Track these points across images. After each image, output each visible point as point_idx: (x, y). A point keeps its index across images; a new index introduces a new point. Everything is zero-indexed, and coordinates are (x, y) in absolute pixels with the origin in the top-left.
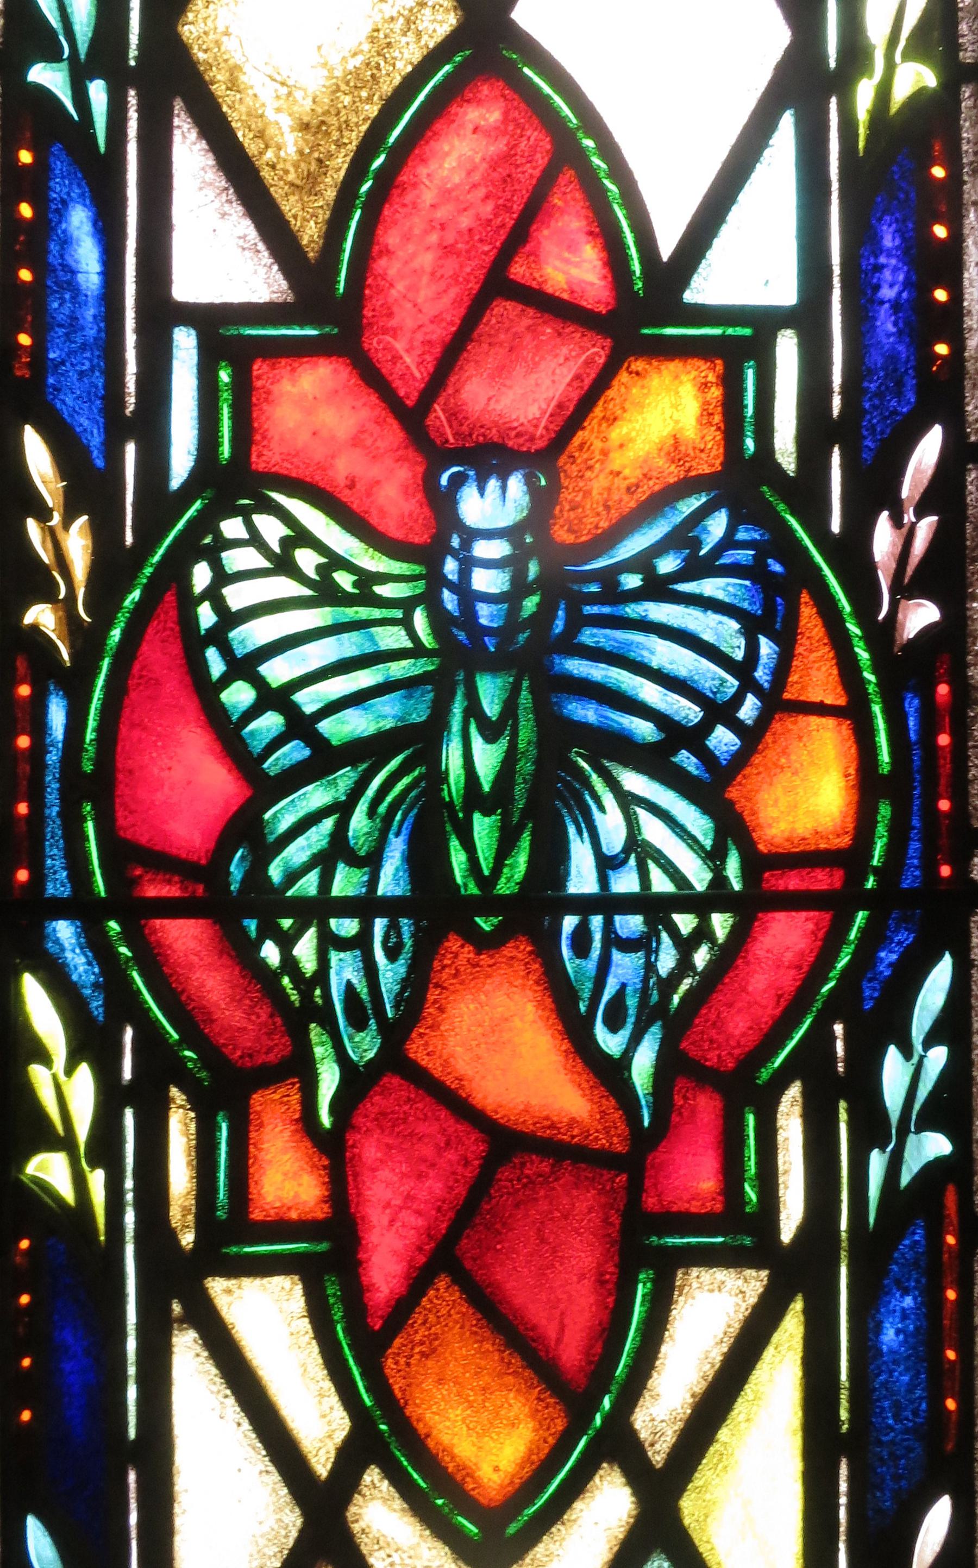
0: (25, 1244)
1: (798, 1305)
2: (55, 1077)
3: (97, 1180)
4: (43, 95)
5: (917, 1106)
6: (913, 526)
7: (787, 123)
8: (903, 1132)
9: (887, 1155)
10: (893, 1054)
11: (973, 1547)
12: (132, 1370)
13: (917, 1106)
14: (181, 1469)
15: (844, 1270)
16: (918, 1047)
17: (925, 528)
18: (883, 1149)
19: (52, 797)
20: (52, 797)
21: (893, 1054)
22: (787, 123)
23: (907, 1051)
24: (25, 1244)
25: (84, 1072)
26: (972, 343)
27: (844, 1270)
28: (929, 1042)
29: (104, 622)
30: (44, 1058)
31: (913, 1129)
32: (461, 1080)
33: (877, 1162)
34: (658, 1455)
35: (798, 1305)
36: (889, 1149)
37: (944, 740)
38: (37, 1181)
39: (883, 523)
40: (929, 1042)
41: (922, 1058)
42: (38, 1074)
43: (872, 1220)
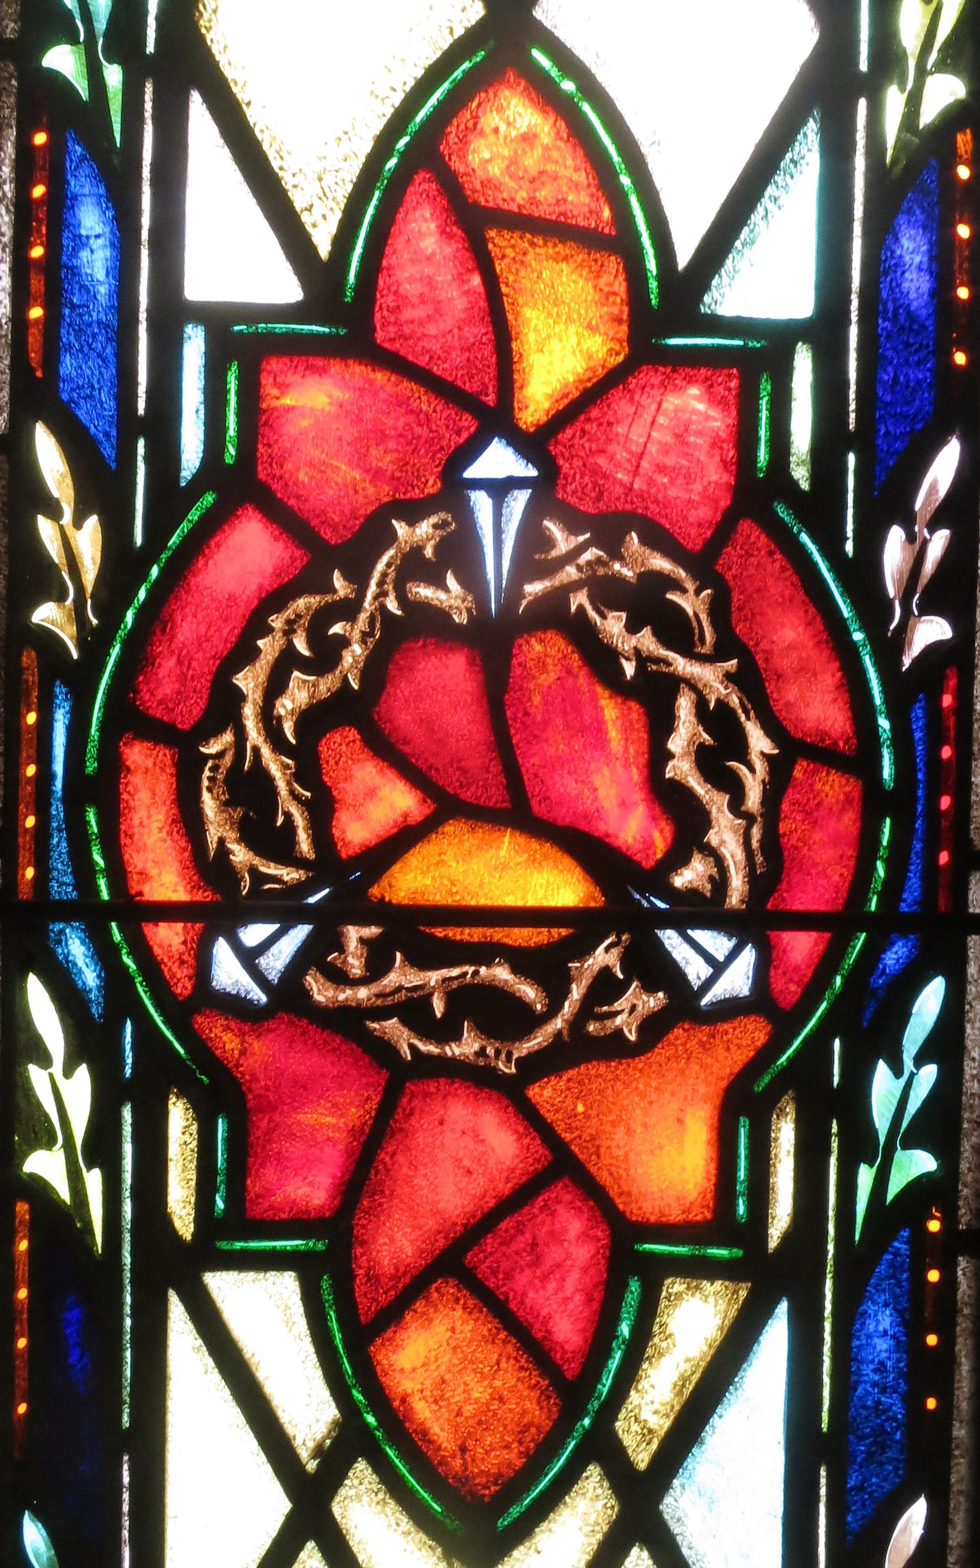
0: (22, 1408)
1: (783, 1308)
2: (62, 528)
3: (93, 1180)
4: (56, 81)
5: (905, 1124)
6: (925, 543)
7: (811, 132)
8: (922, 73)
9: (905, 95)
10: (882, 1070)
11: (973, 638)
12: (127, 1237)
13: (905, 1124)
14: (172, 1376)
15: (829, 1284)
16: (909, 1065)
17: (938, 542)
18: (871, 1166)
19: (57, 809)
20: (57, 809)
21: (882, 1070)
22: (811, 132)
23: (897, 1070)
24: (22, 1408)
25: (83, 1073)
26: (969, 1069)
27: (829, 1284)
28: (920, 1060)
29: (111, 616)
30: (45, 1060)
31: (916, 613)
32: (460, 761)
33: (866, 1176)
34: (642, 1458)
35: (783, 1308)
36: (877, 1164)
37: (945, 802)
38: (34, 1177)
39: (896, 535)
40: (920, 1060)
41: (912, 1075)
42: (37, 1076)
43: (857, 1238)
